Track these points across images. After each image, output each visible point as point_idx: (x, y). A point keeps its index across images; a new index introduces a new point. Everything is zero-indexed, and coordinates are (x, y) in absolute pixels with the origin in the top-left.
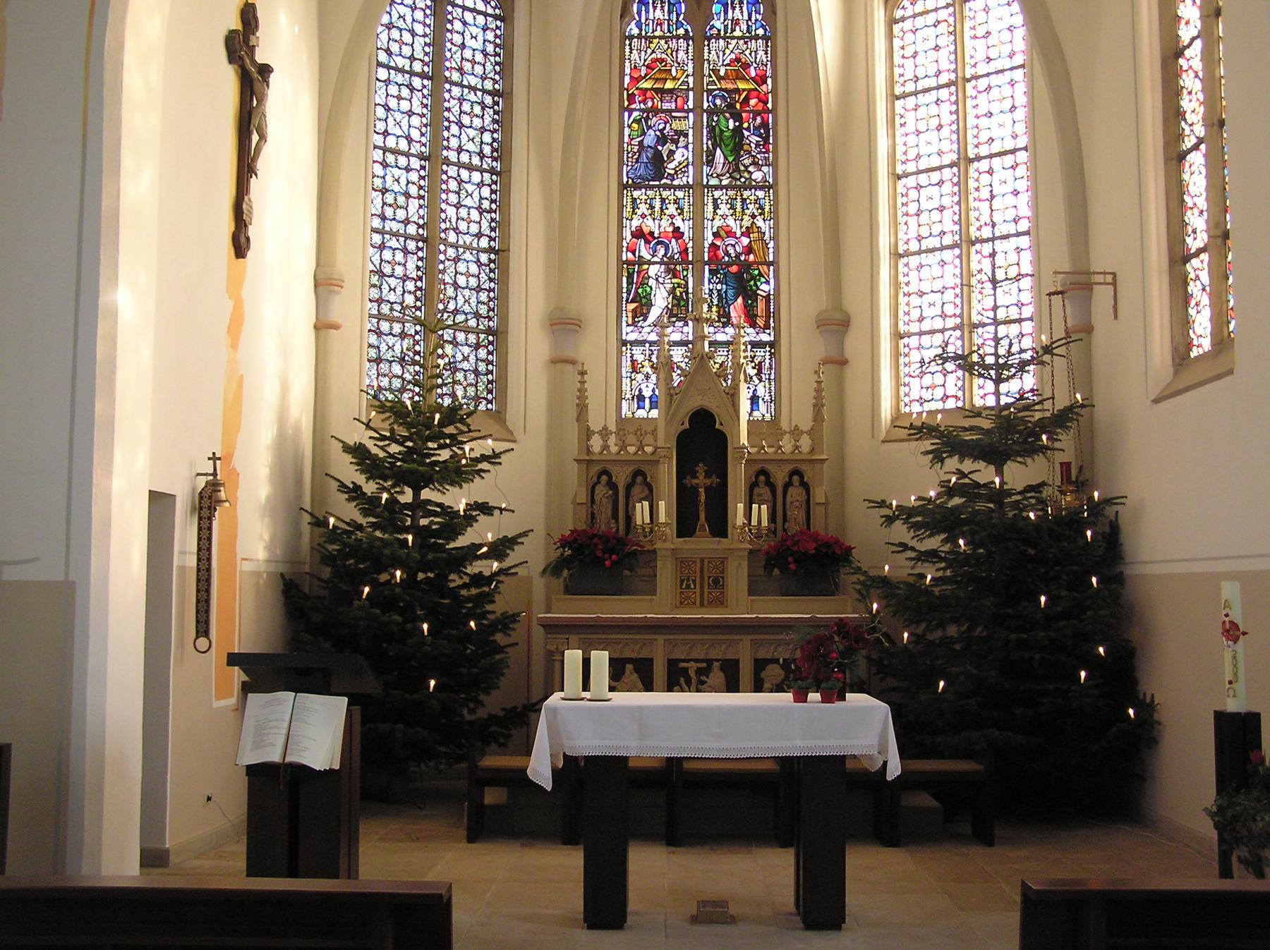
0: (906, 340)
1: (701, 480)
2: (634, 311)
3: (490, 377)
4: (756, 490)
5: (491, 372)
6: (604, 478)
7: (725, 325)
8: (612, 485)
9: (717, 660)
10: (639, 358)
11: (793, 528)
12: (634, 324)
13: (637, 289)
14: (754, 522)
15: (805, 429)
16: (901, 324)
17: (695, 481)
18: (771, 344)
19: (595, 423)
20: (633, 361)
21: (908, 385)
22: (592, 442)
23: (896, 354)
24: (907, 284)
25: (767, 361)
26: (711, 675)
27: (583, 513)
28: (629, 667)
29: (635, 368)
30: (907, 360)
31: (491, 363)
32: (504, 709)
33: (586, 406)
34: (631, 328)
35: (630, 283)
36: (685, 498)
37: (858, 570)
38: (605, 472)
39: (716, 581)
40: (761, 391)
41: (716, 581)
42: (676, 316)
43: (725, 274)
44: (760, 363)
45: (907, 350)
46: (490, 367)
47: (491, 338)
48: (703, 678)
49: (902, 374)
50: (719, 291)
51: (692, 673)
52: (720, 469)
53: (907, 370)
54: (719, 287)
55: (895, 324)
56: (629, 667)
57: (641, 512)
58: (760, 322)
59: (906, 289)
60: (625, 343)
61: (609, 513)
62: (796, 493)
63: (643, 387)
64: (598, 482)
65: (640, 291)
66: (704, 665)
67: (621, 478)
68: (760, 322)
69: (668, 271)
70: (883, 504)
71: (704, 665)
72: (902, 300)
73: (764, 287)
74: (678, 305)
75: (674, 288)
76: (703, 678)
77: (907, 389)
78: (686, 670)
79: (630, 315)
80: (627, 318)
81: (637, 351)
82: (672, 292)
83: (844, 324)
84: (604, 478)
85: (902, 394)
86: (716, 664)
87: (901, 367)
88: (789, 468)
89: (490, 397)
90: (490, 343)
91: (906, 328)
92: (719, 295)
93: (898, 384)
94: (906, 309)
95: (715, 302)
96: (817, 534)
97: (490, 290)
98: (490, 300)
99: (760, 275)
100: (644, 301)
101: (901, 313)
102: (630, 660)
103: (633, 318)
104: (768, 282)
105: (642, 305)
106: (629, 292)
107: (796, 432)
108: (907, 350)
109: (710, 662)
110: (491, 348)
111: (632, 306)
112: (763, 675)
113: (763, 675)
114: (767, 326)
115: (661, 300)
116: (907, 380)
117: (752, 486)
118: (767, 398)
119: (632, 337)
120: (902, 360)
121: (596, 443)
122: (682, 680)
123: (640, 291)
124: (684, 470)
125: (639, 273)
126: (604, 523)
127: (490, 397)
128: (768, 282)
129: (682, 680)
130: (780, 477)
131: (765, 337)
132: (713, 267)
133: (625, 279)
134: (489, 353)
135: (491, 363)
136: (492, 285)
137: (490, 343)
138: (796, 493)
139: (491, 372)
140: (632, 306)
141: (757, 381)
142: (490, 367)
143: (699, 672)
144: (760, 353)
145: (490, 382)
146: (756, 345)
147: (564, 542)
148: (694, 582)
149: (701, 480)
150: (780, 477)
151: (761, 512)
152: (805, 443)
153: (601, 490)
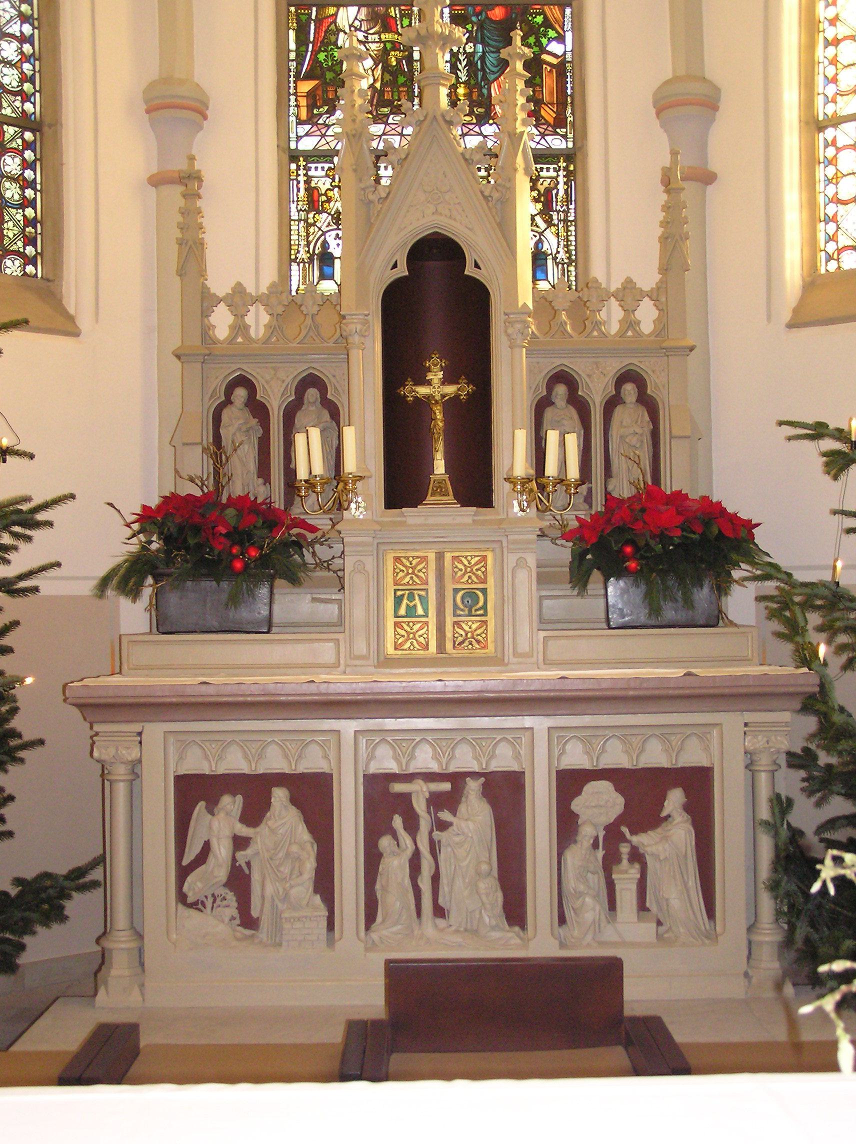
0: (830, 133)
1: (436, 386)
2: (311, 95)
3: (29, 212)
4: (549, 413)
5: (32, 204)
6: (240, 394)
7: (482, 120)
8: (258, 410)
9: (474, 775)
10: (323, 184)
11: (623, 489)
12: (312, 120)
13: (315, 53)
14: (551, 469)
15: (646, 288)
16: (820, 101)
17: (422, 390)
18: (569, 156)
19: (219, 283)
20: (311, 191)
21: (834, 219)
22: (214, 319)
23: (810, 161)
24: (833, 22)
25: (561, 187)
26: (462, 808)
27: (197, 463)
28: (279, 795)
29: (314, 201)
30: (831, 171)
31: (32, 184)
32: (18, 881)
33: (201, 245)
34: (303, 129)
35: (302, 41)
36: (402, 428)
37: (772, 571)
38: (243, 381)
39: (471, 597)
40: (551, 243)
41: (471, 597)
42: (389, 103)
43: (481, 27)
44: (548, 191)
45: (831, 152)
46: (29, 193)
47: (28, 136)
48: (445, 815)
49: (821, 199)
50: (469, 56)
51: (420, 806)
52: (473, 361)
53: (831, 190)
54: (469, 48)
55: (808, 103)
56: (279, 795)
57: (309, 454)
58: (548, 114)
59: (830, 33)
60: (294, 157)
61: (252, 466)
62: (629, 421)
63: (330, 238)
64: (228, 401)
65: (322, 56)
66: (446, 786)
67: (275, 396)
68: (548, 114)
69: (373, 18)
70: (818, 431)
71: (446, 786)
72: (820, 52)
73: (556, 48)
74: (393, 84)
75: (385, 52)
76: (445, 815)
77: (831, 228)
78: (406, 798)
79: (303, 102)
80: (297, 108)
81: (318, 171)
82: (381, 58)
83: (709, 103)
84: (240, 394)
85: (821, 237)
86: (473, 787)
87: (820, 187)
88: (614, 367)
89: (30, 251)
90: (27, 145)
91: (830, 109)
92: (471, 64)
93: (813, 218)
94: (831, 71)
95: (463, 77)
96: (679, 497)
97: (23, 39)
98: (25, 58)
99: (547, 24)
100: (329, 75)
101: (820, 80)
102: (281, 779)
103: (310, 107)
104: (561, 39)
105: (325, 84)
106: (300, 64)
107: (629, 294)
108: (831, 152)
109: (458, 779)
110: (29, 155)
111: (306, 87)
112: (577, 805)
113: (577, 805)
114: (560, 122)
115: (364, 77)
116: (831, 209)
117: (541, 407)
118: (562, 255)
119: (307, 144)
120: (821, 172)
121: (221, 321)
122: (398, 822)
123: (322, 56)
124: (399, 366)
125: (319, 22)
126: (242, 480)
127: (30, 251)
128: (561, 39)
129: (398, 822)
130: (596, 391)
131: (556, 143)
132: (459, 10)
133: (292, 35)
134: (25, 165)
135: (32, 184)
136: (27, 29)
137: (27, 145)
138: (629, 421)
139: (32, 204)
140: (306, 87)
141: (543, 225)
142: (29, 193)
143: (437, 802)
144: (548, 172)
145: (29, 222)
146: (542, 157)
147: (147, 518)
148: (424, 600)
149: (436, 386)
150: (596, 391)
151: (564, 450)
152: (647, 315)
153: (236, 420)
